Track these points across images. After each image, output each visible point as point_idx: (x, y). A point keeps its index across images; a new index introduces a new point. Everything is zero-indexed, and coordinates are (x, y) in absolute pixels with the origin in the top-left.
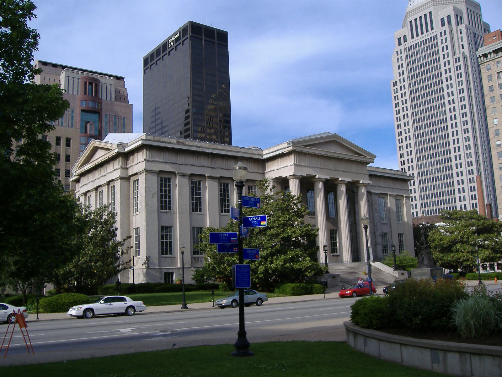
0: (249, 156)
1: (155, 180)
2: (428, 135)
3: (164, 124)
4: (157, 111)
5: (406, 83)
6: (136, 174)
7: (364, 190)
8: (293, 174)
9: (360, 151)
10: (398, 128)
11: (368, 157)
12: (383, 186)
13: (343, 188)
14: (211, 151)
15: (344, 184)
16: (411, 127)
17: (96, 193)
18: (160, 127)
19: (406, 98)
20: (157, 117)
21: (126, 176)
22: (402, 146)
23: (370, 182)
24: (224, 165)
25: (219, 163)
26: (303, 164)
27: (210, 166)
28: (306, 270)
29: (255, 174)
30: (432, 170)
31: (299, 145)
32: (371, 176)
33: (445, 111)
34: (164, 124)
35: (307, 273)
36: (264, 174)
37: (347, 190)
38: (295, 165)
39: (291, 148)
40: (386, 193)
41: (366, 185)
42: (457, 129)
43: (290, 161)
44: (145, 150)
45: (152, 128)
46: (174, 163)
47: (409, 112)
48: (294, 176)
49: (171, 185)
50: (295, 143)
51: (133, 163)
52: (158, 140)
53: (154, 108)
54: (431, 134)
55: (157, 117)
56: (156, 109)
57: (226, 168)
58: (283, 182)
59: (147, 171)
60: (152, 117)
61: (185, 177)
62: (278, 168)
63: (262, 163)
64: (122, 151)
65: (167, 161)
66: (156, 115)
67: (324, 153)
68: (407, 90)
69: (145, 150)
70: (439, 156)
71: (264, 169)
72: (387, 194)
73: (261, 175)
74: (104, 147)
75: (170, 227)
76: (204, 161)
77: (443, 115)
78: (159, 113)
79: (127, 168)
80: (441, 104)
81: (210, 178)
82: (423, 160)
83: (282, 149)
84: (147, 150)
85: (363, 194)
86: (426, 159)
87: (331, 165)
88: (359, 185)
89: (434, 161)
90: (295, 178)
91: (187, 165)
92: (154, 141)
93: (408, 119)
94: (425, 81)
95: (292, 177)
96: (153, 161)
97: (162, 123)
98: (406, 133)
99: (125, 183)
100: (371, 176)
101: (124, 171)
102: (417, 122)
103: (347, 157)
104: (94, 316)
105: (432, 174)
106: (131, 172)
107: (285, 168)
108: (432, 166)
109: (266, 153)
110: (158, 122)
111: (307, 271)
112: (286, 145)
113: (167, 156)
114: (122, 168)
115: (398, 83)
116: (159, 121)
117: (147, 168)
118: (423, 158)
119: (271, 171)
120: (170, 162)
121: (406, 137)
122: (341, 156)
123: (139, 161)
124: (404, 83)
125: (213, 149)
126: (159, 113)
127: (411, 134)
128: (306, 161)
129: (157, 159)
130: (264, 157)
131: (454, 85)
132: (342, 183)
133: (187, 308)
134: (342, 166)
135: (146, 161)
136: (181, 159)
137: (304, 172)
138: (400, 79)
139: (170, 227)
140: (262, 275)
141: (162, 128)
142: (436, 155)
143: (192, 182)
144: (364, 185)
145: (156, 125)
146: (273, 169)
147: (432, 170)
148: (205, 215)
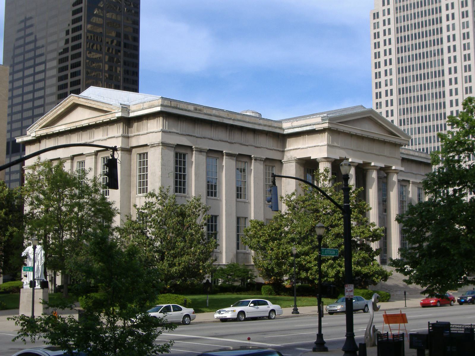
0: (270, 129)
1: (171, 154)
2: (417, 91)
3: (39, 44)
4: (28, 23)
5: (392, 16)
6: (146, 145)
7: (395, 178)
8: (326, 156)
9: (393, 129)
10: (376, 78)
11: (403, 138)
12: (414, 172)
13: (374, 175)
14: (231, 122)
15: (376, 169)
16: (394, 77)
17: (72, 163)
18: (32, 46)
19: (390, 37)
20: (28, 31)
21: (127, 147)
22: (381, 103)
23: (403, 169)
24: (243, 139)
25: (237, 137)
26: (335, 144)
27: (229, 141)
28: (373, 275)
29: (274, 151)
30: (419, 138)
31: (335, 122)
32: (404, 160)
33: (443, 60)
34: (39, 44)
35: (374, 278)
36: (283, 151)
37: (379, 178)
38: (328, 145)
39: (326, 125)
40: (408, 179)
41: (397, 172)
42: (456, 86)
43: (323, 140)
44: (161, 119)
45: (20, 47)
46: (192, 136)
47: (393, 57)
48: (327, 159)
49: (187, 162)
50: (331, 120)
51: (138, 131)
52: (175, 106)
53: (23, 18)
54: (421, 90)
55: (28, 31)
56: (26, 20)
57: (245, 143)
58: (309, 166)
59: (164, 145)
60: (19, 31)
61: (203, 153)
62: (304, 146)
63: (282, 138)
64: (125, 115)
65: (184, 133)
66: (26, 28)
67: (359, 133)
68: (392, 26)
69: (161, 119)
70: (430, 121)
71: (284, 146)
72: (409, 181)
73: (279, 153)
74: (95, 106)
75: (216, 217)
76: (222, 134)
77: (439, 65)
78: (32, 26)
79: (128, 137)
80: (438, 50)
81: (228, 155)
82: (408, 124)
83: (314, 125)
84: (163, 117)
85: (394, 182)
86: (411, 123)
87: (365, 146)
88: (391, 171)
89: (422, 127)
90: (328, 161)
91: (204, 138)
92: (170, 107)
93: (391, 67)
94: (418, 16)
95: (323, 160)
96: (170, 132)
97: (35, 41)
98: (386, 85)
99: (126, 155)
100: (404, 160)
101: (125, 140)
102: (403, 72)
103: (382, 138)
104: (247, 319)
105: (419, 144)
106: (134, 142)
107: (317, 149)
108: (419, 133)
109: (288, 128)
110: (28, 39)
111: (374, 276)
112: (319, 120)
113: (182, 125)
114: (123, 136)
115: (381, 14)
116: (32, 38)
117: (164, 141)
118: (408, 121)
119: (293, 149)
120: (188, 133)
121: (387, 91)
122: (376, 137)
123: (149, 131)
124: (389, 17)
125: (234, 120)
126: (32, 26)
127: (394, 87)
128: (340, 141)
129: (174, 130)
130: (286, 132)
131: (457, 27)
132: (374, 169)
133: (298, 313)
134: (376, 148)
135: (163, 131)
136: (199, 131)
137: (337, 155)
138: (384, 11)
139: (216, 217)
140: (333, 279)
141: (36, 48)
142: (426, 119)
143: (176, 154)
144: (396, 171)
145: (25, 44)
146: (296, 147)
147: (419, 138)
148: (220, 200)
